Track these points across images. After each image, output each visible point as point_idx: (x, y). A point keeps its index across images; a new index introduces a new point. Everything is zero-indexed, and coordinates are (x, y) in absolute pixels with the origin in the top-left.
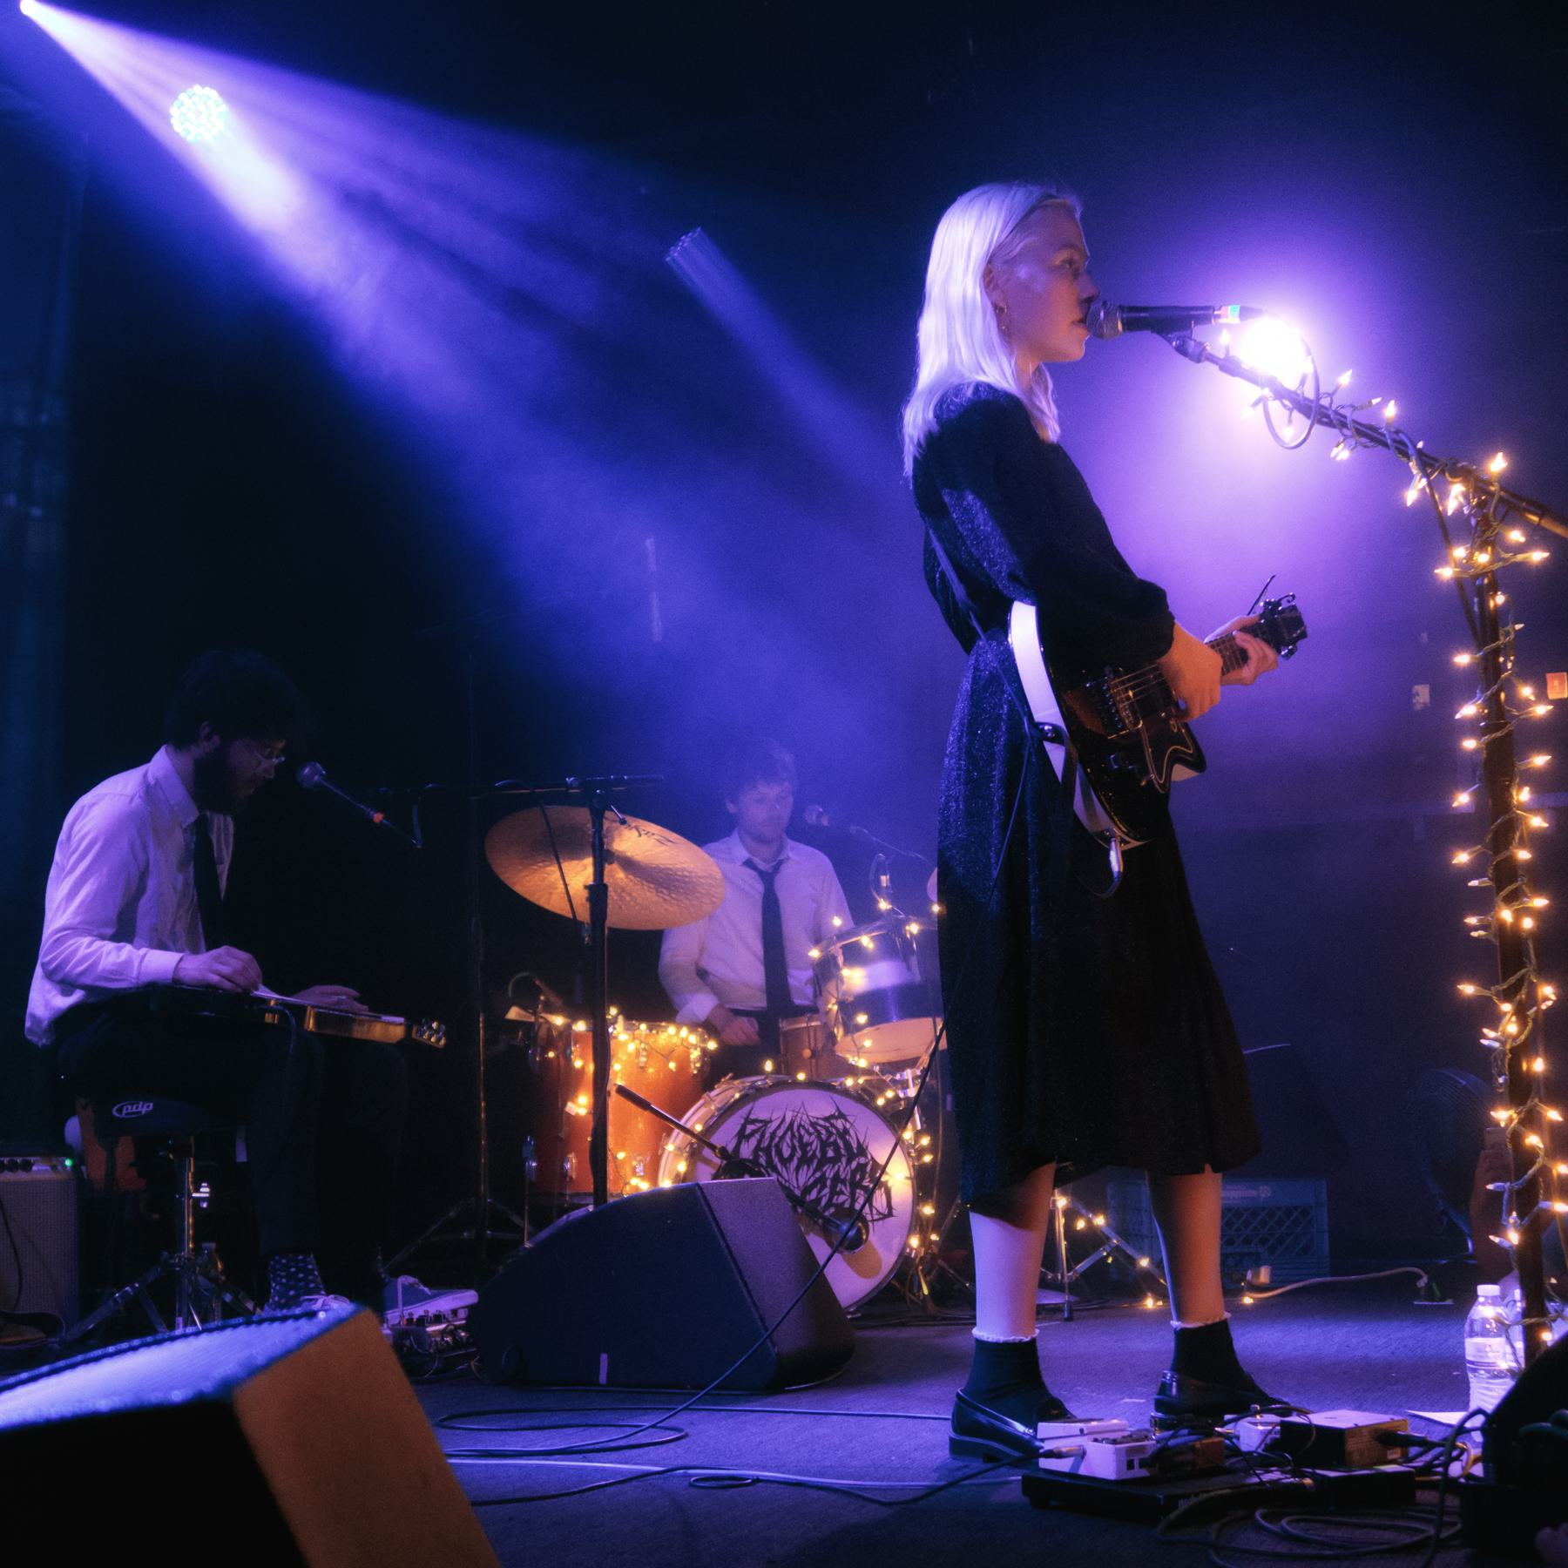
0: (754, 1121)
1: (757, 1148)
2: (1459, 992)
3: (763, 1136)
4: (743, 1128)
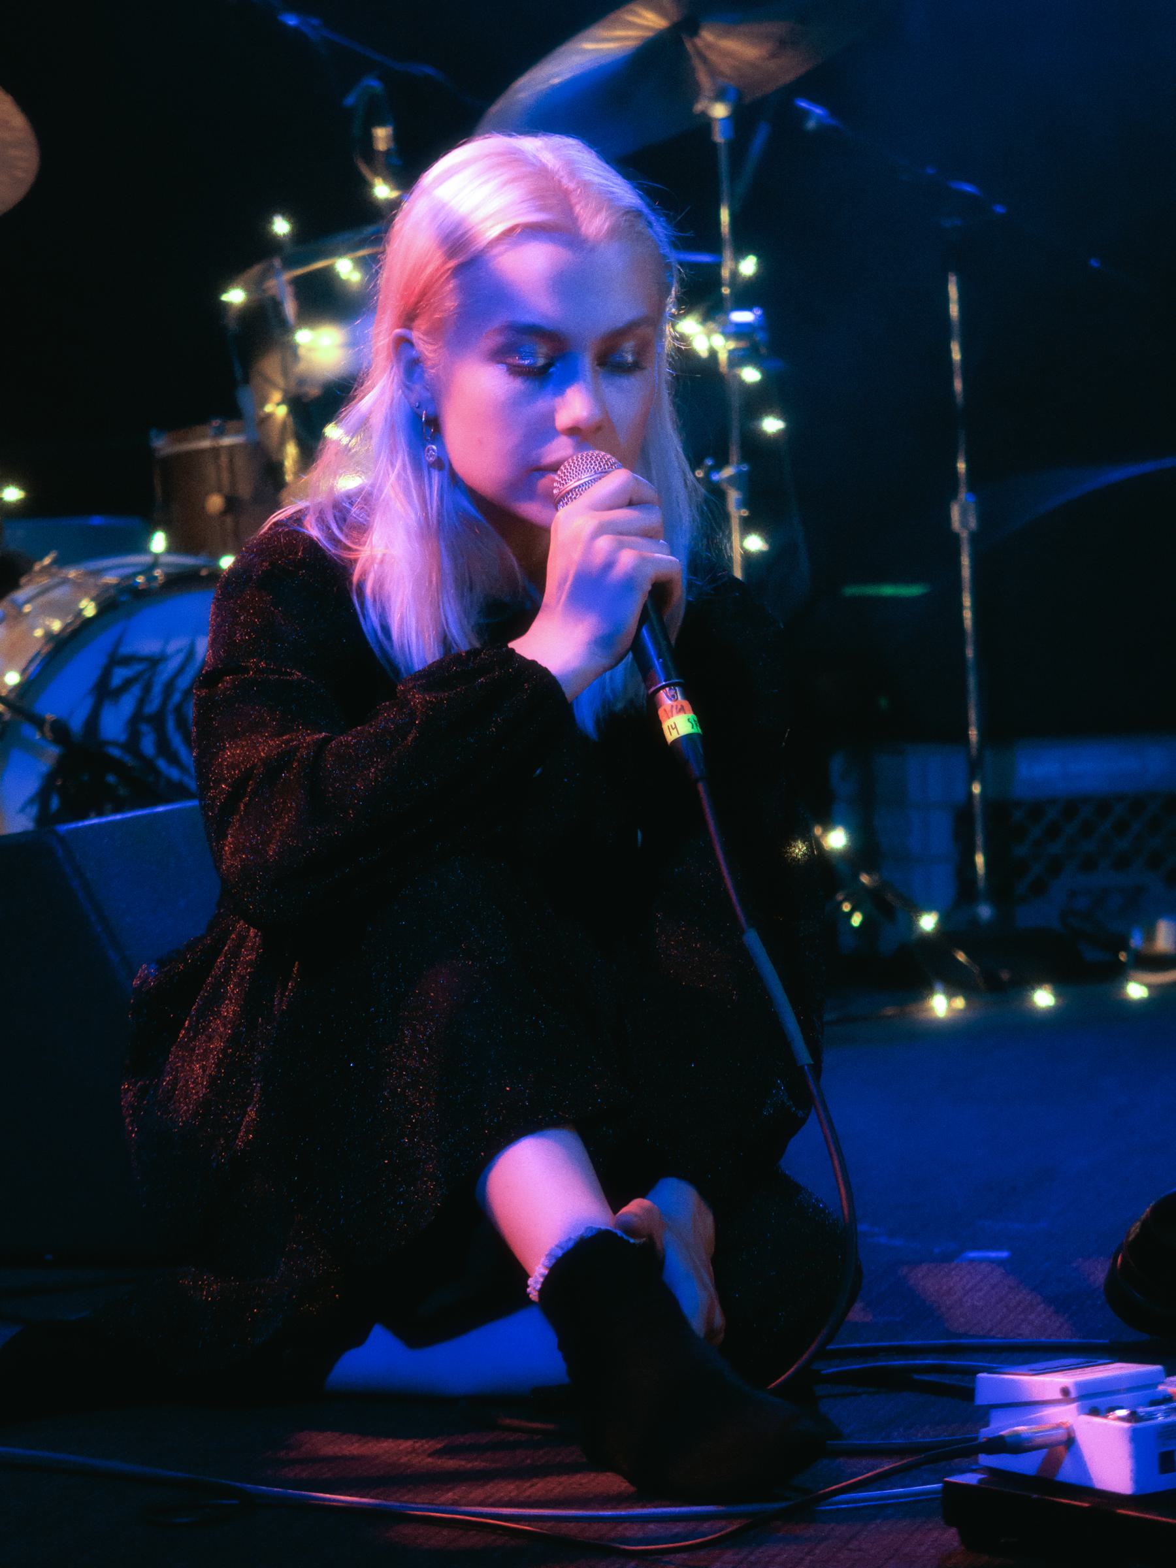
0: (127, 661)
1: (136, 719)
2: (22, 485)
3: (147, 689)
4: (106, 674)
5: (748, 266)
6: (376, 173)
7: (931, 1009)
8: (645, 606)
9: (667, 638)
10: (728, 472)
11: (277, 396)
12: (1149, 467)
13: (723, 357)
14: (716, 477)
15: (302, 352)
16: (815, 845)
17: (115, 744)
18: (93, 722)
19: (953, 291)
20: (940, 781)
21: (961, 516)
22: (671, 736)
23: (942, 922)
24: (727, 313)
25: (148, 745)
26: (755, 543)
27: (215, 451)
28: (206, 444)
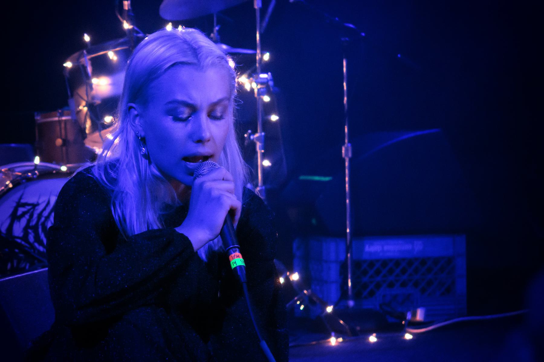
1: (26, 229)
3: (31, 216)
5: (267, 57)
6: (124, 19)
7: (329, 342)
8: (226, 217)
9: (233, 227)
10: (257, 135)
11: (84, 103)
12: (419, 133)
13: (256, 91)
14: (252, 137)
15: (94, 86)
16: (287, 279)
17: (18, 238)
18: (10, 228)
19: (345, 63)
20: (333, 251)
21: (346, 151)
22: (233, 266)
23: (334, 309)
24: (259, 74)
25: (31, 238)
26: (267, 163)
27: (60, 122)
28: (56, 119)
